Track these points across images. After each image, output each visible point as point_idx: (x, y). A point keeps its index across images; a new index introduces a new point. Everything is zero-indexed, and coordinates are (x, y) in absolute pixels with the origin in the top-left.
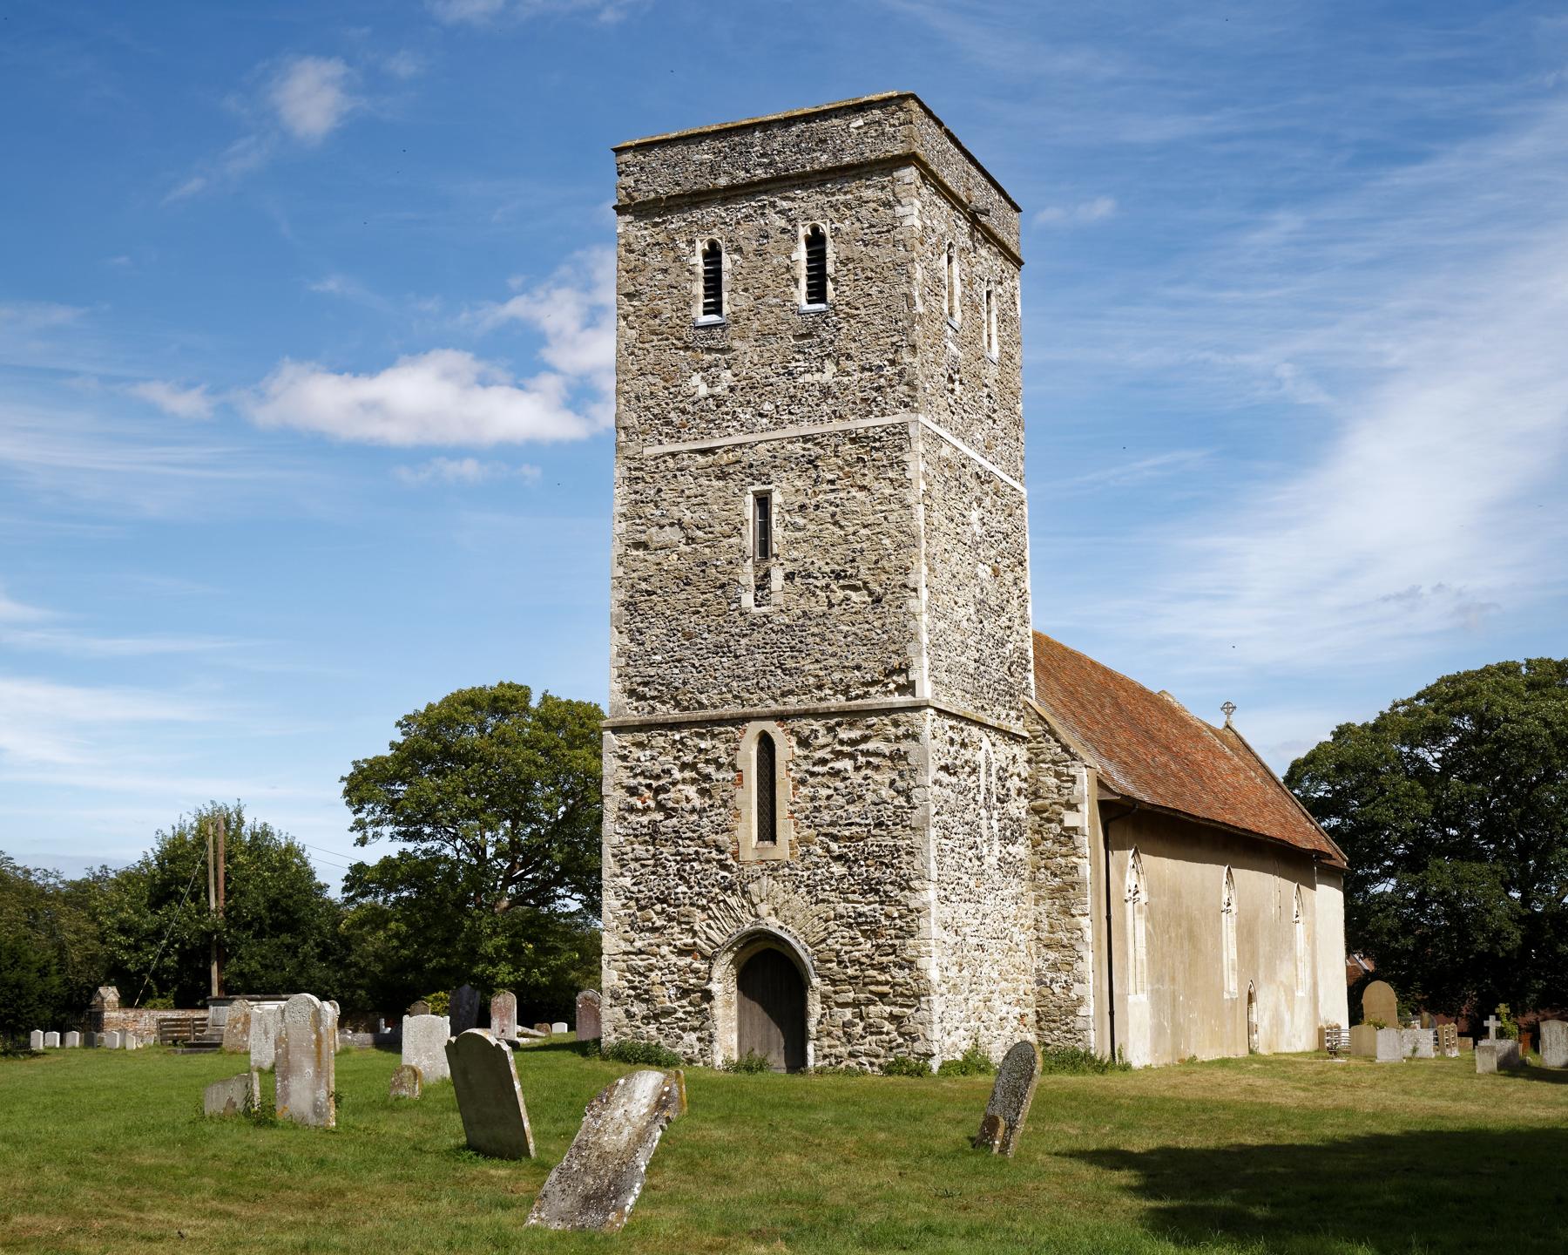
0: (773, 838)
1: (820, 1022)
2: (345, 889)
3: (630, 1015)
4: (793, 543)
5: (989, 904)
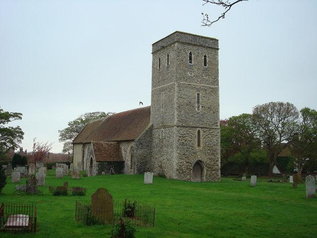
3: (179, 173)
4: (203, 102)
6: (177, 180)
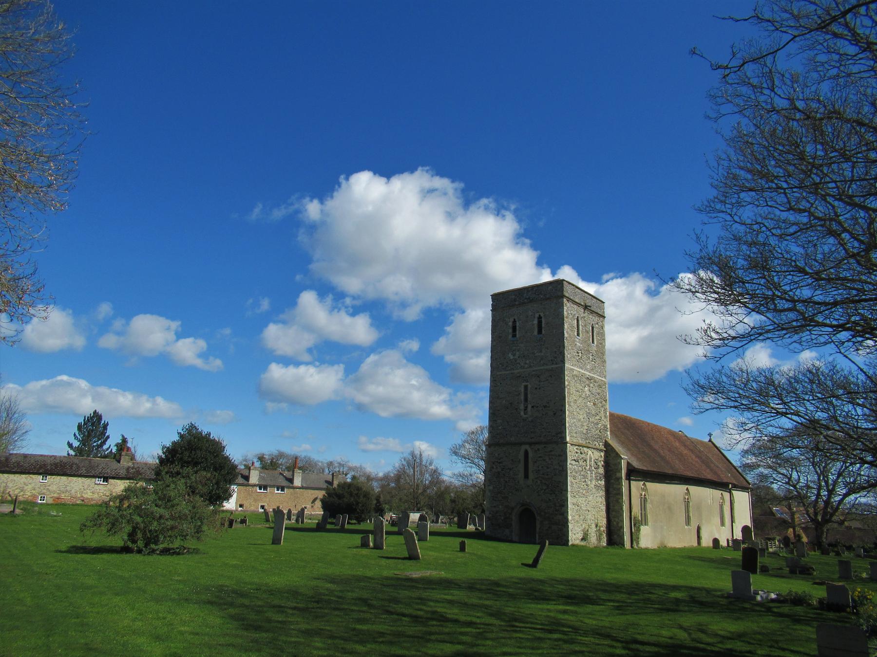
2: (745, 453)
5: (590, 498)
6: (192, 369)
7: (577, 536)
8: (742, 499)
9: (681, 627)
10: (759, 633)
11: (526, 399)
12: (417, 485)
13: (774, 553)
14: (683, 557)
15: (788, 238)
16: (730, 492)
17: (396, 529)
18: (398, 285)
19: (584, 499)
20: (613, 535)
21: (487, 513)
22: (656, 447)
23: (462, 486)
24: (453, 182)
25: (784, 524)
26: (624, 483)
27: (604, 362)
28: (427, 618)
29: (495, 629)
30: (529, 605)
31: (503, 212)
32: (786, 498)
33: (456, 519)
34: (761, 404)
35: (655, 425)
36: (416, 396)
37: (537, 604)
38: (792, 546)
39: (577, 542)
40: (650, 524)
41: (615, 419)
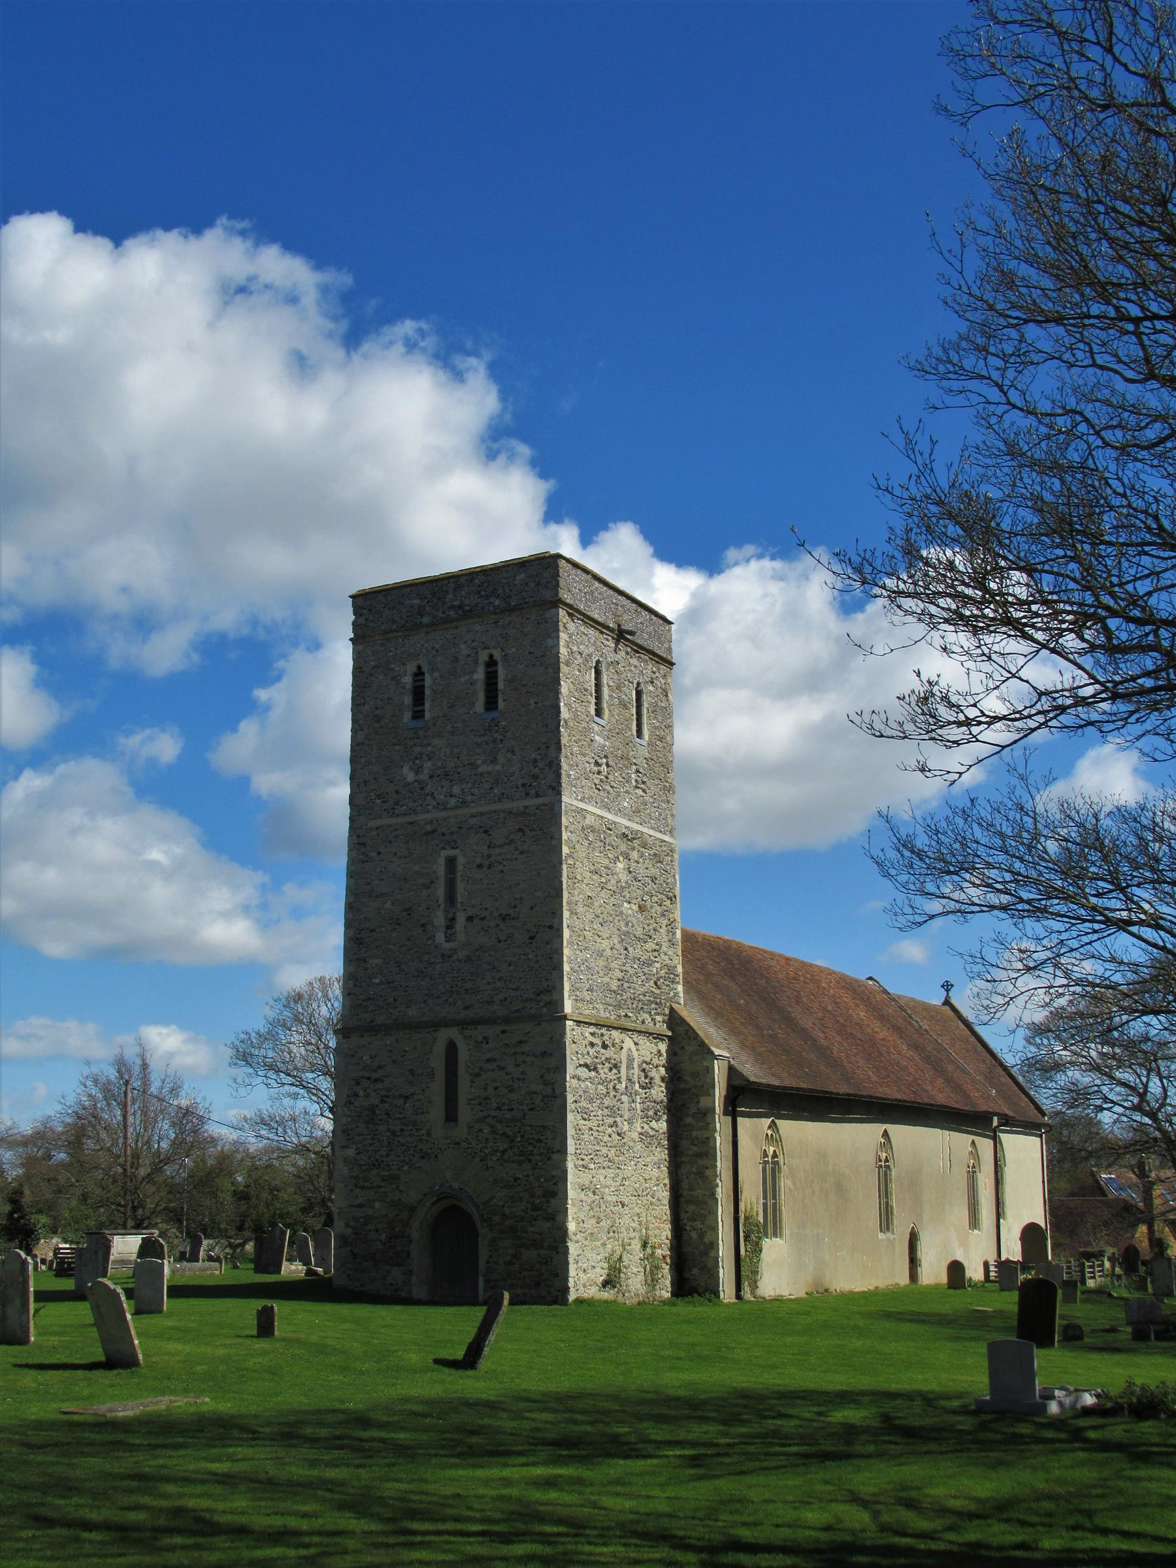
0: (455, 1120)
1: (488, 1262)
5: (629, 1169)
7: (591, 1274)
8: (1025, 1154)
9: (855, 1499)
10: (1050, 1497)
11: (451, 898)
12: (136, 1156)
13: (1100, 1292)
14: (870, 1315)
15: (1143, 454)
16: (995, 1138)
17: (68, 1284)
18: (125, 567)
19: (611, 1173)
20: (690, 1268)
21: (339, 1224)
22: (806, 1022)
23: (268, 1150)
24: (318, 267)
25: (1128, 1215)
26: (721, 1124)
27: (669, 789)
28: (155, 1529)
29: (351, 1544)
30: (452, 1473)
31: (460, 361)
32: (1130, 1147)
33: (250, 1247)
34: (1068, 898)
35: (804, 965)
36: (159, 893)
37: (475, 1466)
38: (1142, 1269)
39: (593, 1292)
40: (787, 1231)
41: (696, 948)
